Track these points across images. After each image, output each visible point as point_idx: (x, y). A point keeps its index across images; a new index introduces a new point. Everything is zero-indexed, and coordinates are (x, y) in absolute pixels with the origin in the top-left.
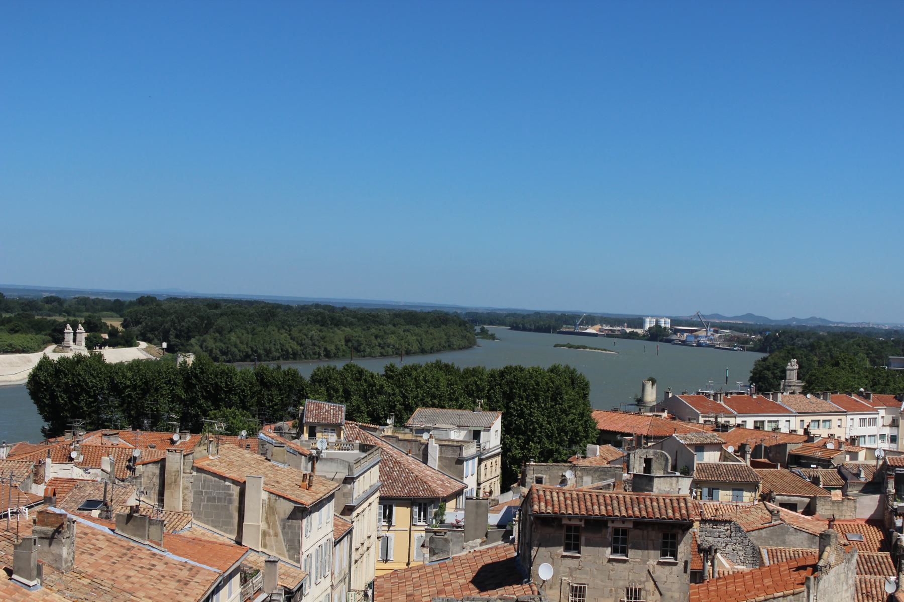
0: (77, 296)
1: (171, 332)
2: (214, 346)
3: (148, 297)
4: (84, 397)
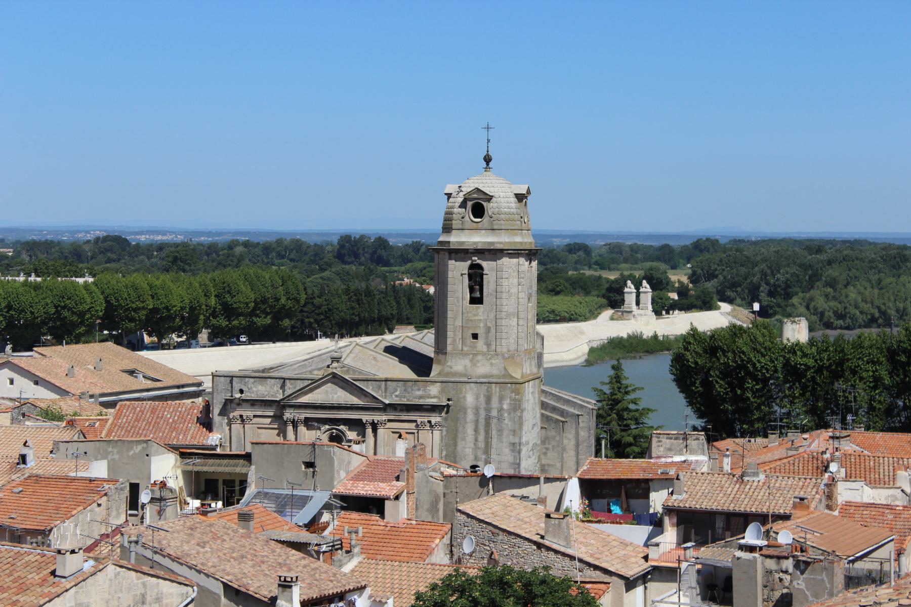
0: (609, 242)
1: (762, 288)
2: (826, 306)
3: (708, 239)
4: (750, 383)
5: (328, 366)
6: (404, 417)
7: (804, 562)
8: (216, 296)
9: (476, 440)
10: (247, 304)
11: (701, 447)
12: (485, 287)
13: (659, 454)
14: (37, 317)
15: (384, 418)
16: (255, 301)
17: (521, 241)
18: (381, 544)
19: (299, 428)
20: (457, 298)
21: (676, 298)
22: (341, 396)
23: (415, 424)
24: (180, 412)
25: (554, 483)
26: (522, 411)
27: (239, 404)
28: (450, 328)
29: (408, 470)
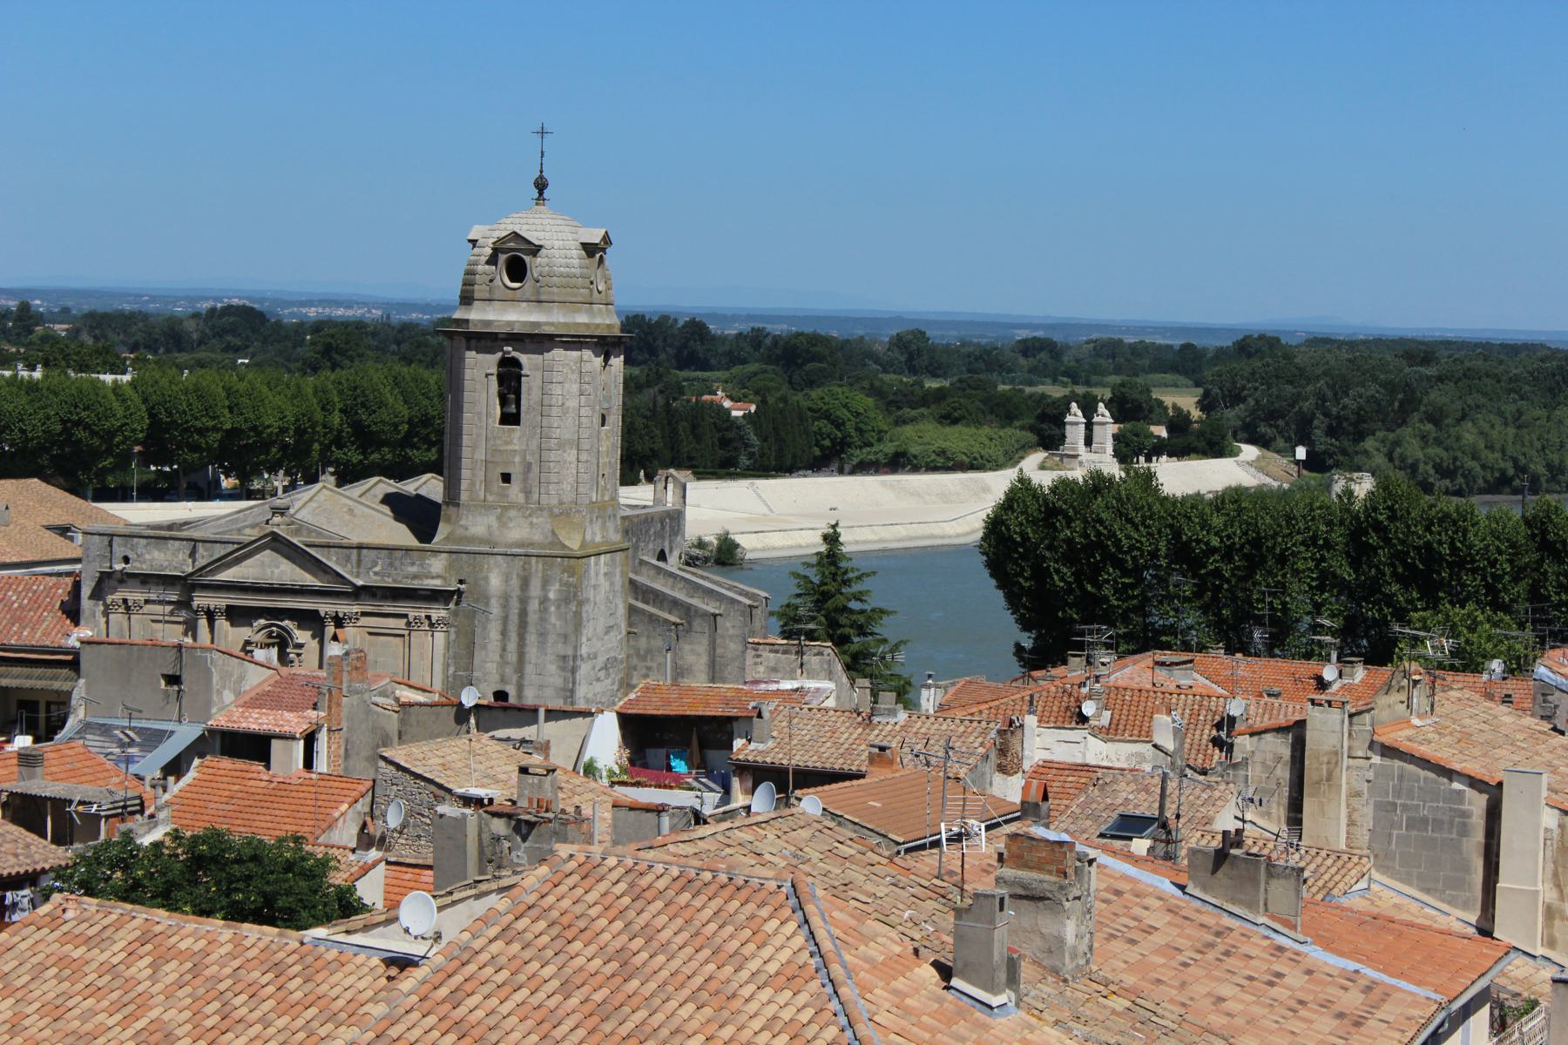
0: (1094, 336)
1: (1316, 422)
3: (1262, 337)
4: (1111, 572)
5: (267, 522)
6: (388, 608)
7: (527, 822)
8: (341, 411)
9: (504, 649)
10: (396, 426)
11: (826, 666)
12: (523, 396)
13: (757, 676)
14: (32, 439)
15: (356, 609)
16: (410, 422)
17: (586, 321)
18: (255, 810)
19: (217, 623)
20: (480, 413)
21: (1164, 434)
22: (285, 571)
23: (405, 620)
24: (35, 592)
25: (574, 720)
26: (581, 604)
27: (121, 581)
28: (465, 462)
29: (330, 691)
